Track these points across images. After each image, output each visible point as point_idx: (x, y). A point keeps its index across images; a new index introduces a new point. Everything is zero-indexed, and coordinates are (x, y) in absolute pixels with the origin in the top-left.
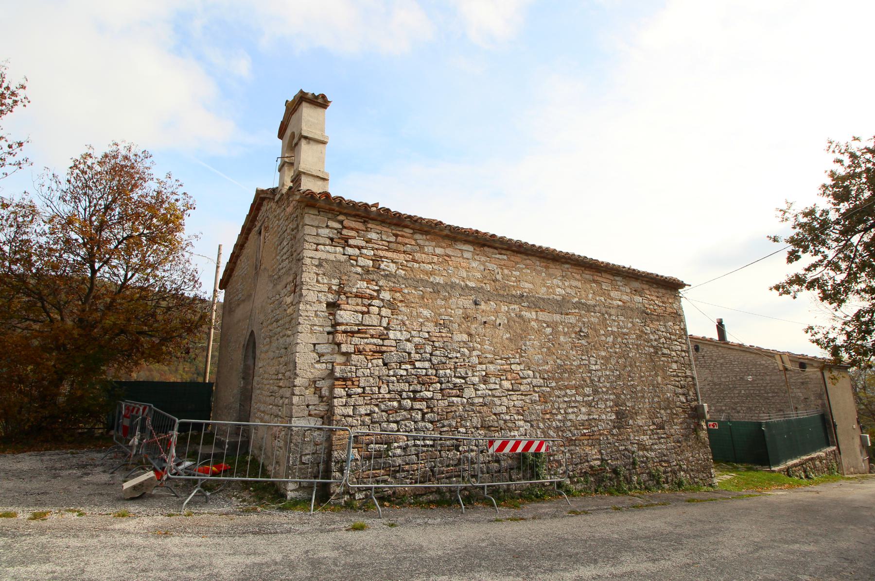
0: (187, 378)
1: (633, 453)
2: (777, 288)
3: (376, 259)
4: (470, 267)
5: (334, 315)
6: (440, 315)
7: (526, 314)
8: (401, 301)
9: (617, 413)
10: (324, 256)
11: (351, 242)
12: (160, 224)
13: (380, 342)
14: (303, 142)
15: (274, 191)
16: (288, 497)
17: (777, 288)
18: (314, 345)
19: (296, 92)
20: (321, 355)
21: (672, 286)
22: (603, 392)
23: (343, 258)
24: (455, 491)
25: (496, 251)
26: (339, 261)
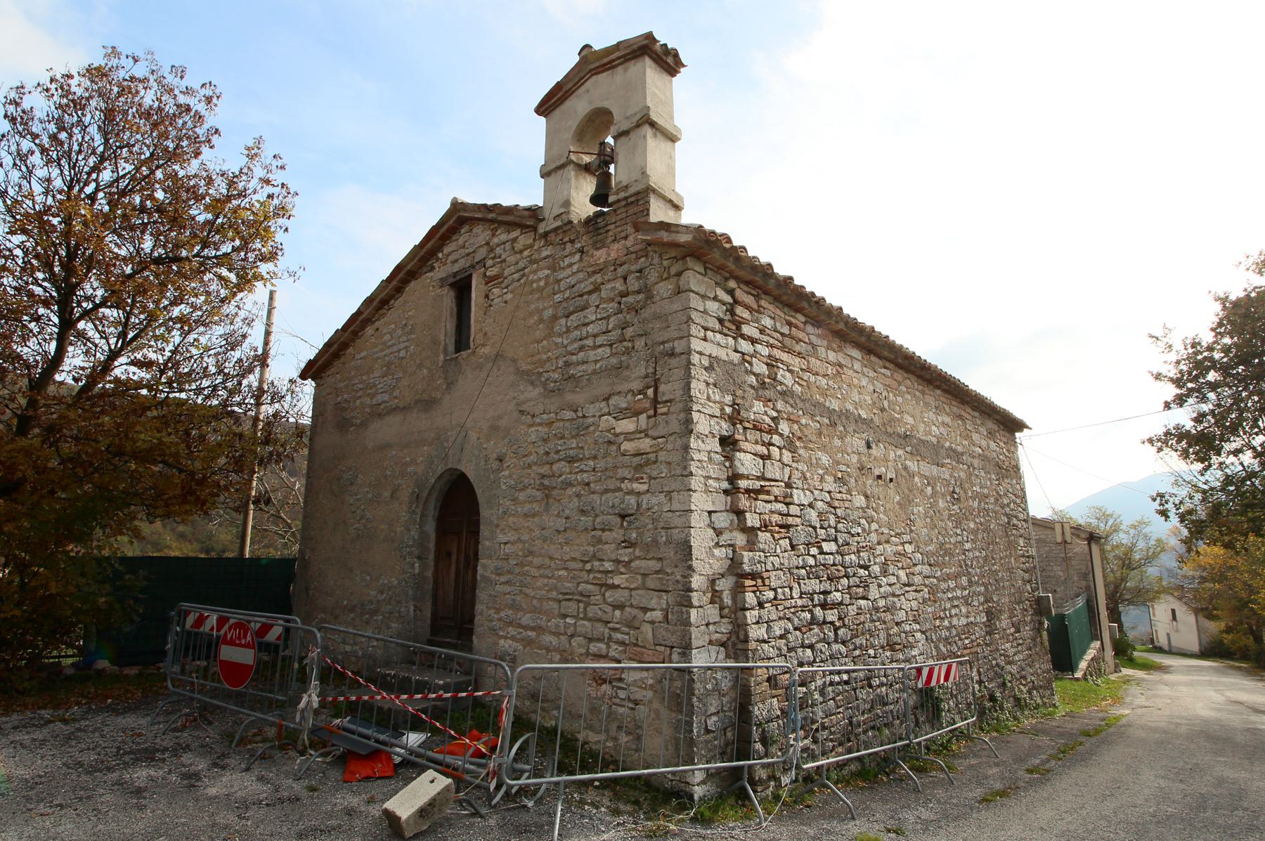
0: (138, 553)
2: (1151, 441)
3: (772, 363)
4: (861, 386)
5: (729, 458)
6: (838, 463)
7: (912, 465)
8: (800, 438)
10: (715, 351)
11: (746, 329)
12: (223, 236)
13: (781, 507)
14: (648, 131)
15: (533, 212)
16: (696, 797)
17: (1151, 441)
18: (710, 513)
20: (718, 533)
21: (1010, 425)
23: (736, 357)
24: (378, 724)
25: (881, 363)
26: (731, 363)
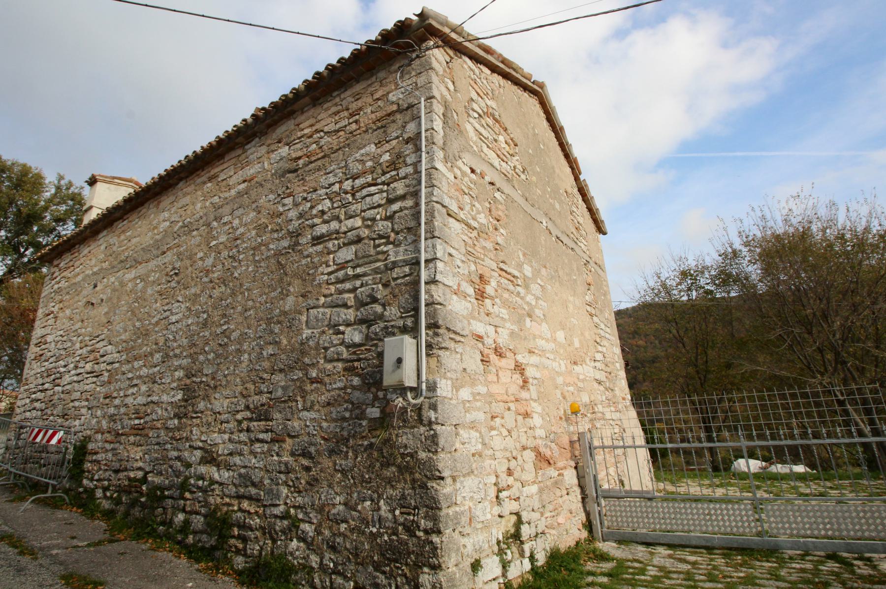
1: (188, 465)
9: (186, 389)
19: (90, 176)
22: (176, 356)
